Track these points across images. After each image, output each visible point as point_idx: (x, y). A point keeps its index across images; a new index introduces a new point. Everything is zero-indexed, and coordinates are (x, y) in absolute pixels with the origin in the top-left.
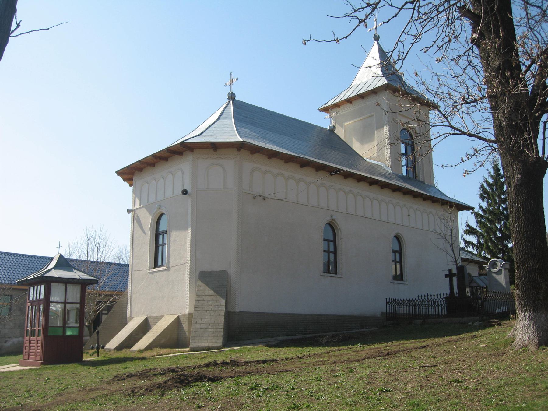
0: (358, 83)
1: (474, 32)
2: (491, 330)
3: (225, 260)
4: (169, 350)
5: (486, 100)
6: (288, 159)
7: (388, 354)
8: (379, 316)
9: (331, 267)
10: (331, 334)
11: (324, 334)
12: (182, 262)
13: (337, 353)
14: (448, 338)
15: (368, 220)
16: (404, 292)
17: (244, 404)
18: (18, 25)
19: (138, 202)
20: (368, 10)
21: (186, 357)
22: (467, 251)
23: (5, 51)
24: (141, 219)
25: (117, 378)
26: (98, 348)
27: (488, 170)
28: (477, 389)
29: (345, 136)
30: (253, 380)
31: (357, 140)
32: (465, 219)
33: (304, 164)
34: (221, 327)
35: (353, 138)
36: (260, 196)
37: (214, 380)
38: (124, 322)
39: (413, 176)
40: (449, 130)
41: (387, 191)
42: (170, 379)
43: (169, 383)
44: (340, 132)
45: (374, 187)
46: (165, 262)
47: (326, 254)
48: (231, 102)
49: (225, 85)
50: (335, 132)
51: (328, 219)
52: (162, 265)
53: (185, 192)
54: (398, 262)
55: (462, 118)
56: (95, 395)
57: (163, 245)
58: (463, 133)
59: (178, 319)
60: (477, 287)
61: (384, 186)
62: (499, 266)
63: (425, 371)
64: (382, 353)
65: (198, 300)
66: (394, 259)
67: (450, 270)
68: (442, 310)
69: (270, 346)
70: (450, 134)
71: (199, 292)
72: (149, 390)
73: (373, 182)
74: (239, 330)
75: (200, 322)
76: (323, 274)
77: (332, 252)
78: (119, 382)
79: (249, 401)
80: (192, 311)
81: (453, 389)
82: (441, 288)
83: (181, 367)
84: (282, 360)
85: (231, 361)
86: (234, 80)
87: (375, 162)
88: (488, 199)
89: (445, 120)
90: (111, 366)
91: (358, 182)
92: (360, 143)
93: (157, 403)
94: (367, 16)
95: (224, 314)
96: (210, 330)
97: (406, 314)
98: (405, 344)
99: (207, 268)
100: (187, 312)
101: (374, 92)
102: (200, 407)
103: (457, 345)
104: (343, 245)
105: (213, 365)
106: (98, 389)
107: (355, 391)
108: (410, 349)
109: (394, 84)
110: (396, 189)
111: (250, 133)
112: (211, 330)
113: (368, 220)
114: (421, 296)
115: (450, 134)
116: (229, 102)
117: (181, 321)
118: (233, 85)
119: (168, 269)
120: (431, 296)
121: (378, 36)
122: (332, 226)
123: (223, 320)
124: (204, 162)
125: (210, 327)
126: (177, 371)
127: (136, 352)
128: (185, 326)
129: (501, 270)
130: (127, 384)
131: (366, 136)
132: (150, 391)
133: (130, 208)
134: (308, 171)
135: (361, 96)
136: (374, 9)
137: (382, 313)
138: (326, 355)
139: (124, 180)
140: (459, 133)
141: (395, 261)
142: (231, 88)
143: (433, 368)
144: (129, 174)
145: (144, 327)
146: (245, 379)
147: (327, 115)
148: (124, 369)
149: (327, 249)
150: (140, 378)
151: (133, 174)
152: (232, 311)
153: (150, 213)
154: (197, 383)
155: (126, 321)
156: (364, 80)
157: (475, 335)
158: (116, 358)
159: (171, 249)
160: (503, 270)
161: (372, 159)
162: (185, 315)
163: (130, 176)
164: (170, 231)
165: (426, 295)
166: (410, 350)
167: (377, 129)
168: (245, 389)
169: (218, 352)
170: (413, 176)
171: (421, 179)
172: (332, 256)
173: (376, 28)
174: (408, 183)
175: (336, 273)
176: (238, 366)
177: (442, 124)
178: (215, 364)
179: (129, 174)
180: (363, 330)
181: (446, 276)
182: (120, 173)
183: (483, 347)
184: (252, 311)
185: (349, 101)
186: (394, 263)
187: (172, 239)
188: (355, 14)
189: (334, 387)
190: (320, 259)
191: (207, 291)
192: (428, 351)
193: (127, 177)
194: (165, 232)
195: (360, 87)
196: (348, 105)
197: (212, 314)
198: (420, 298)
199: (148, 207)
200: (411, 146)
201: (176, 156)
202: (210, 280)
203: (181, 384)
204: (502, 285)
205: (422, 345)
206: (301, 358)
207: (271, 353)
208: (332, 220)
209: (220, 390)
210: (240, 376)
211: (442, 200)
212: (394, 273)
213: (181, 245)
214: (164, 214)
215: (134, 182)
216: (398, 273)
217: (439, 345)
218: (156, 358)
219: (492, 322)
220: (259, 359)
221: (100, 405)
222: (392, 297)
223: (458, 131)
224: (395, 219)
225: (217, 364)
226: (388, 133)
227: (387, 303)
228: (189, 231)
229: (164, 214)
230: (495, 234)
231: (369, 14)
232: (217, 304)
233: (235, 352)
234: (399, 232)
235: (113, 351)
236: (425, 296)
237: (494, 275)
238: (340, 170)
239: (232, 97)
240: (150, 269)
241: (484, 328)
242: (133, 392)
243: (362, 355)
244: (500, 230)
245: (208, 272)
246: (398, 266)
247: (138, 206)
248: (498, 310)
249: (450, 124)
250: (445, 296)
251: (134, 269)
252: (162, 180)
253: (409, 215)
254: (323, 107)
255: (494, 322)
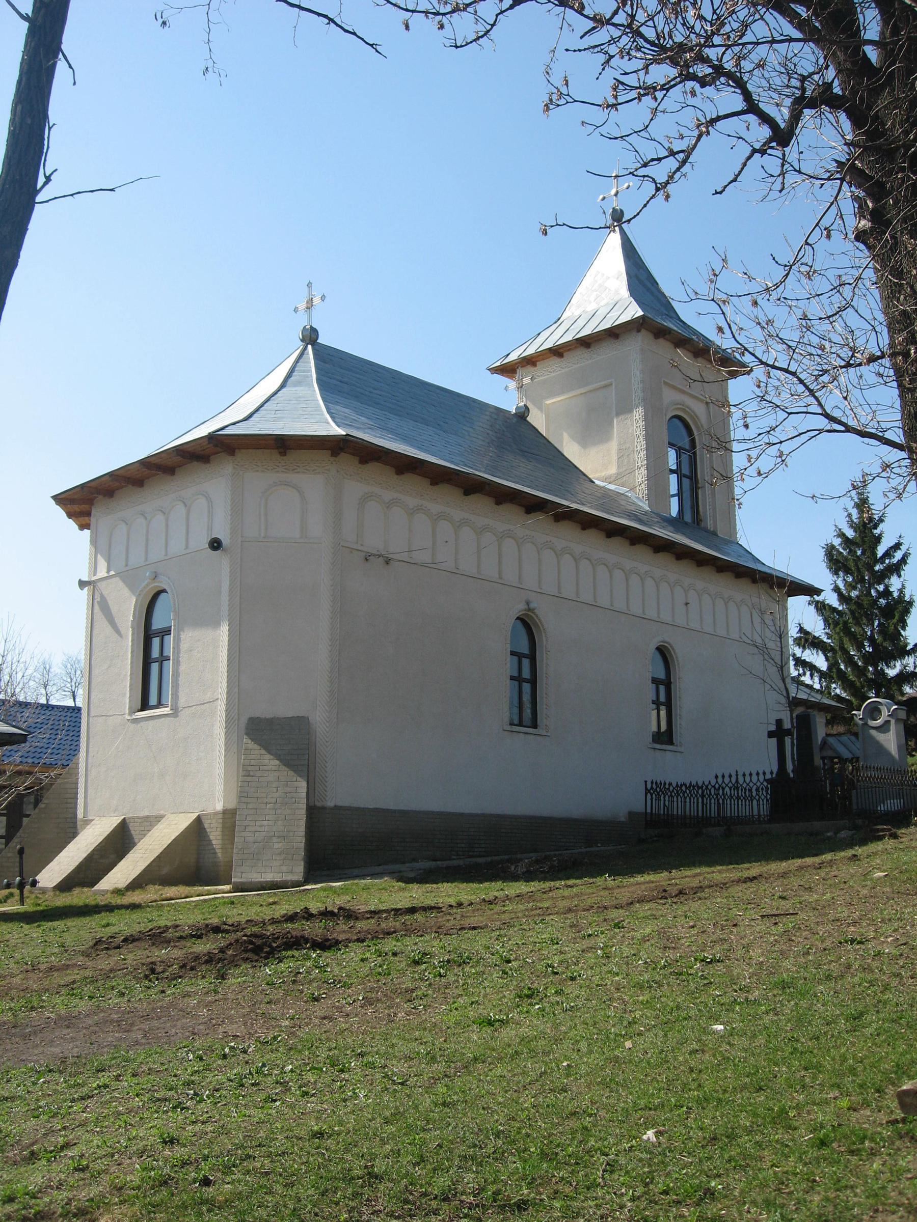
0: (577, 313)
1: (862, 216)
2: (878, 846)
3: (303, 694)
4: (182, 890)
5: (886, 362)
6: (438, 477)
7: (681, 892)
8: (623, 819)
9: (527, 716)
10: (534, 856)
11: (519, 856)
12: (208, 696)
13: (567, 892)
14: (798, 862)
15: (611, 612)
16: (675, 768)
17: (412, 991)
18: (48, 179)
19: (102, 565)
20: (671, 164)
21: (232, 903)
22: (803, 684)
23: (28, 233)
24: (110, 603)
25: (100, 945)
26: (21, 886)
27: (846, 509)
28: (901, 955)
29: (547, 429)
30: (411, 945)
31: (572, 437)
32: (801, 614)
33: (471, 487)
34: (299, 839)
35: (565, 435)
36: (380, 556)
37: (324, 945)
38: (70, 831)
39: (693, 517)
40: (823, 423)
41: (642, 551)
42: (231, 944)
43: (230, 952)
44: (537, 419)
45: (616, 541)
46: (168, 697)
47: (516, 683)
48: (310, 347)
49: (296, 310)
50: (528, 419)
51: (519, 608)
52: (159, 705)
53: (215, 545)
54: (662, 704)
55: (845, 398)
56: (70, 979)
57: (163, 659)
58: (848, 429)
59: (198, 821)
60: (832, 758)
61: (636, 538)
62: (885, 713)
63: (776, 924)
64: (665, 891)
65: (246, 779)
66: (655, 699)
67: (779, 722)
68: (760, 807)
69: (408, 881)
70: (821, 431)
71: (247, 762)
72: (189, 966)
73: (613, 531)
74: (336, 845)
75: (253, 829)
76: (509, 728)
77: (526, 681)
78: (110, 952)
79: (423, 985)
80: (232, 805)
81: (850, 953)
82: (760, 760)
83: (230, 922)
84: (451, 906)
85: (340, 909)
86: (317, 300)
87: (612, 487)
88: (847, 571)
89: (811, 400)
90: (71, 922)
91: (584, 529)
92: (579, 443)
93: (216, 992)
94: (671, 177)
95: (304, 812)
96: (276, 846)
97: (668, 815)
98: (708, 873)
99: (264, 710)
100: (219, 807)
101: (614, 333)
102: (316, 999)
103: (823, 875)
104: (552, 664)
105: (304, 918)
106: (67, 967)
107: (646, 963)
108: (725, 884)
109: (655, 322)
110: (661, 546)
111: (354, 416)
112: (278, 846)
113: (611, 612)
114: (723, 776)
115: (821, 431)
116: (305, 349)
117: (206, 826)
118: (314, 312)
119: (175, 712)
120: (744, 775)
121: (622, 211)
122: (527, 624)
123: (303, 823)
124: (258, 478)
125: (275, 840)
126: (227, 932)
127: (109, 895)
128: (215, 836)
129: (889, 721)
130: (134, 956)
131: (593, 429)
132: (192, 969)
133: (85, 579)
134: (481, 502)
135: (585, 343)
136: (684, 162)
137: (631, 814)
138: (545, 896)
139: (70, 515)
140: (843, 428)
141: (657, 703)
142: (310, 318)
143: (792, 918)
144: (81, 503)
145: (120, 842)
146: (390, 944)
147: (512, 384)
148: (104, 926)
149: (516, 674)
150: (153, 944)
151: (90, 502)
152: (318, 804)
153: (132, 589)
154: (290, 953)
155: (75, 827)
156: (591, 308)
157: (855, 856)
158: (65, 907)
159: (182, 668)
160: (893, 721)
161: (604, 480)
162: (216, 813)
163: (84, 507)
164: (179, 630)
165: (734, 774)
166: (723, 886)
167: (618, 414)
168: (401, 963)
169: (297, 892)
170: (693, 517)
171: (710, 525)
172: (526, 687)
173: (616, 195)
174: (684, 534)
175: (535, 726)
176: (357, 919)
177: (804, 410)
178: (308, 915)
179: (81, 503)
180: (588, 849)
181: (771, 734)
182: (62, 499)
183: (880, 878)
184: (362, 805)
185: (557, 352)
186: (654, 706)
187: (184, 646)
188: (642, 172)
189: (597, 957)
190: (501, 693)
191: (266, 762)
192: (764, 886)
193: (76, 508)
194: (167, 631)
195: (581, 323)
196: (555, 361)
197: (279, 811)
198: (720, 780)
199: (128, 576)
200: (689, 453)
201: (195, 463)
202: (272, 737)
203: (257, 954)
204: (889, 754)
205: (746, 874)
206: (490, 903)
207: (416, 894)
208: (529, 610)
209: (349, 961)
210: (377, 938)
211: (754, 571)
212: (654, 728)
213: (204, 659)
214: (164, 591)
215: (93, 520)
216: (664, 727)
217: (784, 875)
218: (162, 905)
219: (878, 831)
220: (399, 907)
221: (91, 998)
222: (660, 778)
223: (838, 424)
224: (659, 613)
225: (312, 915)
226: (642, 423)
227: (647, 791)
228: (224, 629)
229: (164, 591)
230: (860, 646)
231: (675, 173)
232: (288, 790)
233: (334, 891)
234: (667, 639)
235: (52, 894)
236: (730, 776)
237: (873, 733)
238: (547, 501)
239: (310, 337)
240: (132, 712)
241: (863, 842)
242: (153, 971)
243: (624, 895)
244: (872, 640)
245: (267, 720)
246: (663, 713)
247: (102, 572)
248: (881, 808)
249: (824, 410)
250: (768, 776)
251: (92, 714)
252: (160, 517)
253: (687, 604)
254: (498, 364)
255: (883, 830)
